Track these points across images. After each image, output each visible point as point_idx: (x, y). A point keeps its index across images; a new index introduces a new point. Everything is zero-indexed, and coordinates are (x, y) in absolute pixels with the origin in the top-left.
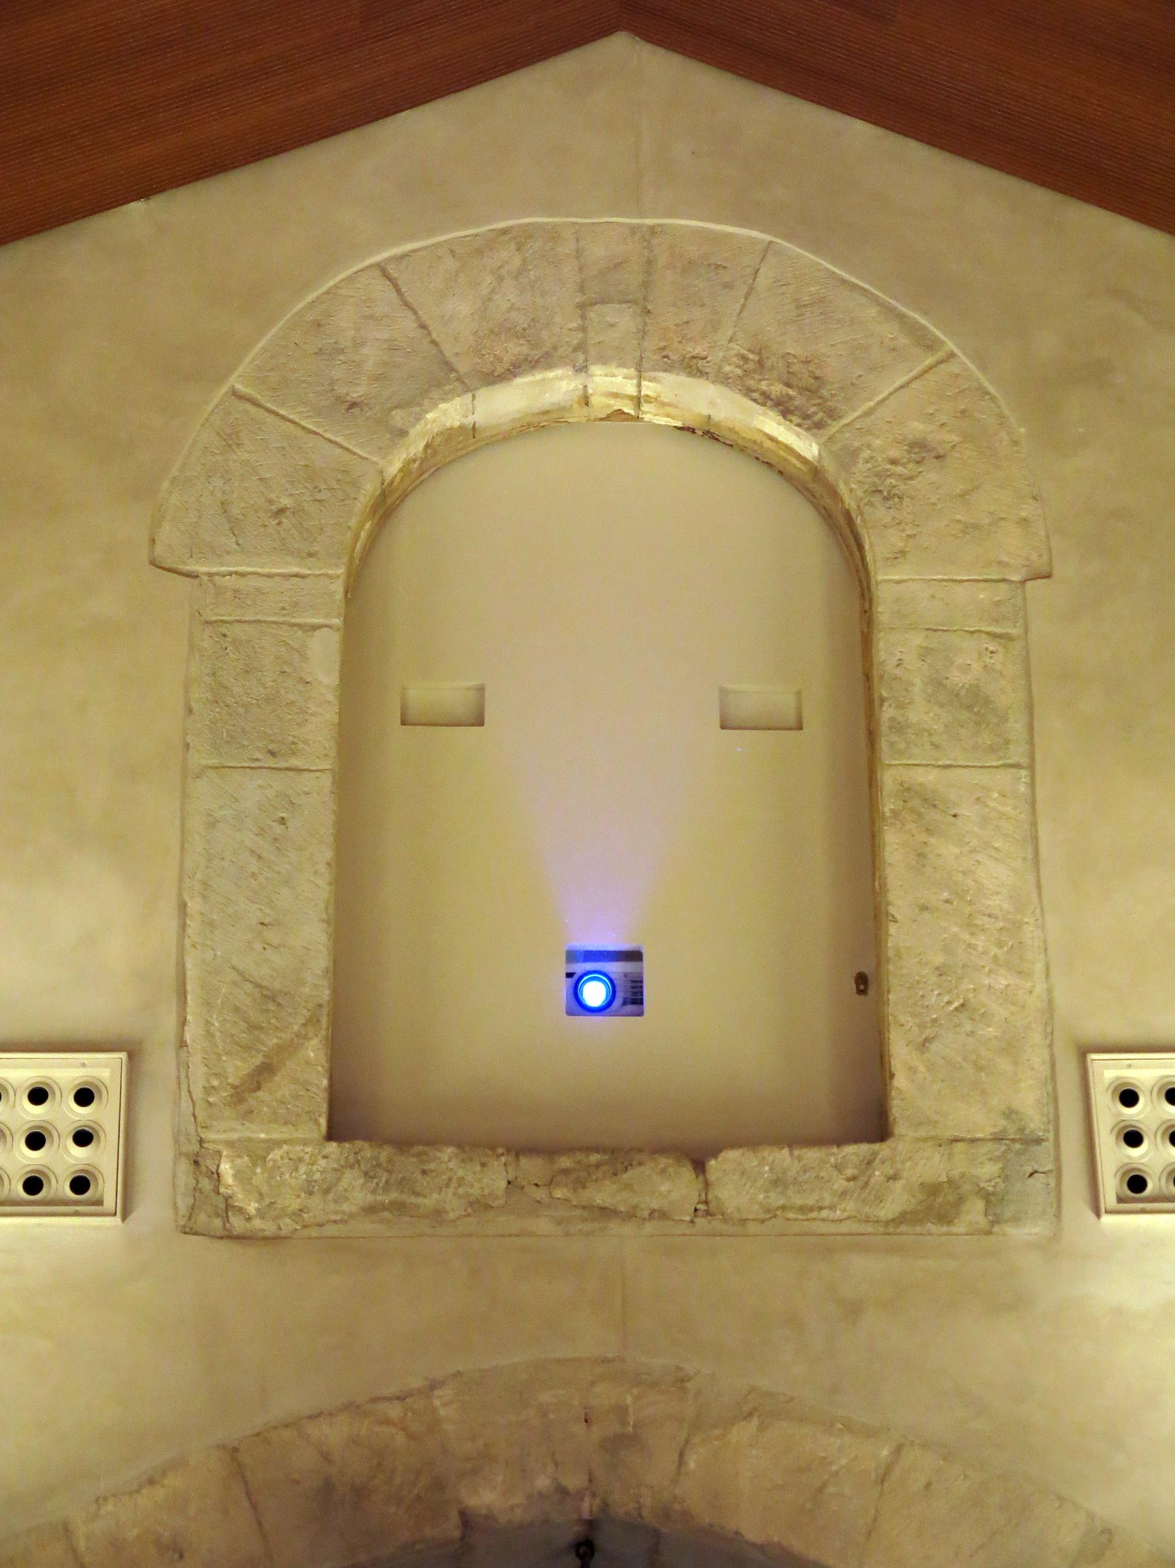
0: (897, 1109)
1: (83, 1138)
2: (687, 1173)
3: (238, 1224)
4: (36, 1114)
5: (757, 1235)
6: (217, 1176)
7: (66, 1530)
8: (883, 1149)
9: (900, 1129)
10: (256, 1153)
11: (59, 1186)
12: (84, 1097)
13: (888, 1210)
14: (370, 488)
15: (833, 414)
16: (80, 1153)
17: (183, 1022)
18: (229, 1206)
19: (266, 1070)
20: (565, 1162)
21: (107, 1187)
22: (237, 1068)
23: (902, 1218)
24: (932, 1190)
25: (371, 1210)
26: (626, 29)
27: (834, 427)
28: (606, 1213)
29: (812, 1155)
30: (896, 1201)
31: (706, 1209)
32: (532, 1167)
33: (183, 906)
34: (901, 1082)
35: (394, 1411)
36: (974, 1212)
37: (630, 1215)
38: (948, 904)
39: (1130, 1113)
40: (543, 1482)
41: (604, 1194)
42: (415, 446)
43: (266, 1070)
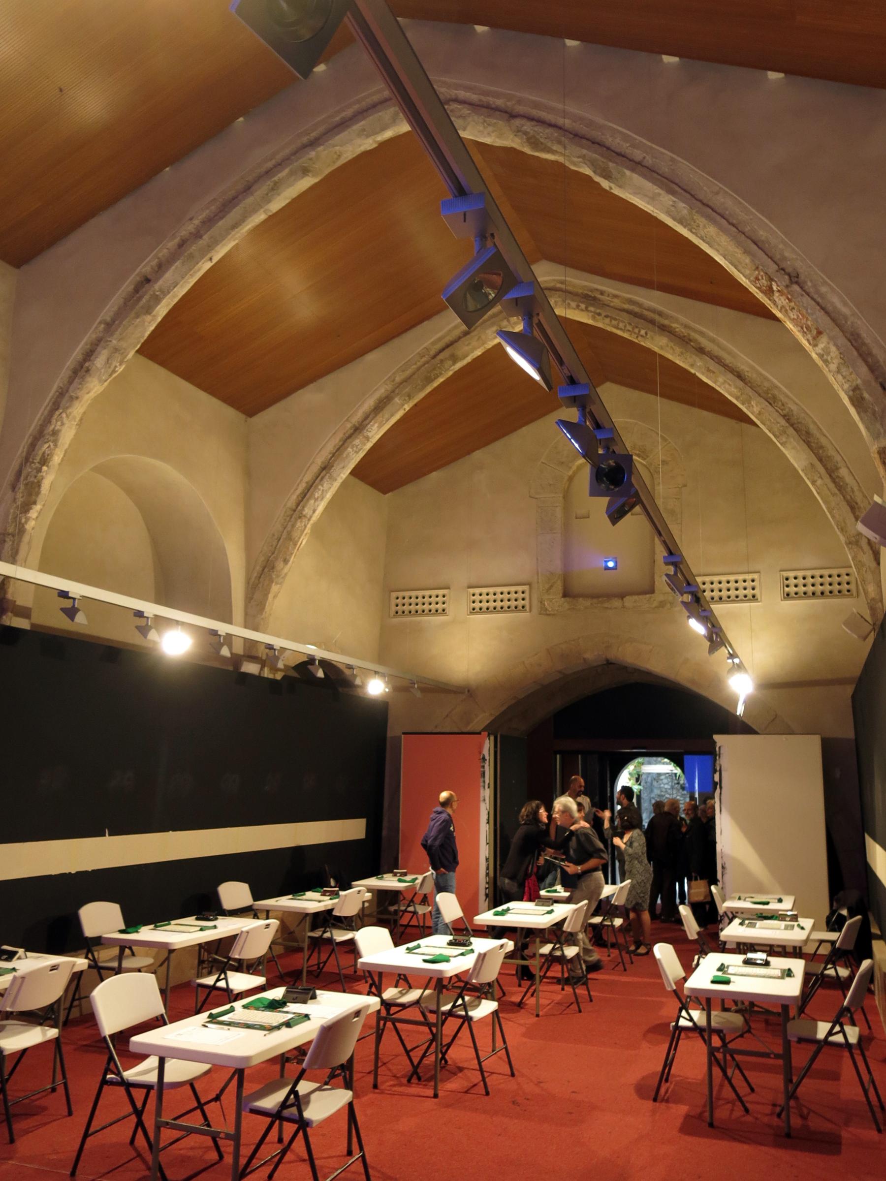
0: (656, 589)
1: (523, 599)
2: (620, 601)
3: (548, 612)
4: (501, 596)
5: (623, 156)
6: (544, 605)
7: (523, 662)
8: (653, 595)
9: (656, 592)
10: (550, 600)
11: (520, 608)
12: (523, 593)
13: (654, 605)
14: (566, 478)
15: (648, 456)
16: (523, 602)
17: (538, 579)
18: (546, 609)
19: (551, 586)
20: (600, 599)
21: (527, 608)
22: (547, 586)
23: (656, 607)
24: (661, 602)
25: (569, 609)
26: (656, 871)
27: (648, 459)
28: (607, 608)
29: (641, 597)
30: (655, 604)
31: (623, 607)
32: (595, 601)
33: (537, 559)
34: (656, 583)
35: (573, 642)
36: (668, 605)
37: (611, 608)
38: (214, 1096)
39: (737, 585)
40: (596, 653)
41: (606, 605)
42: (574, 468)
43: (551, 586)
